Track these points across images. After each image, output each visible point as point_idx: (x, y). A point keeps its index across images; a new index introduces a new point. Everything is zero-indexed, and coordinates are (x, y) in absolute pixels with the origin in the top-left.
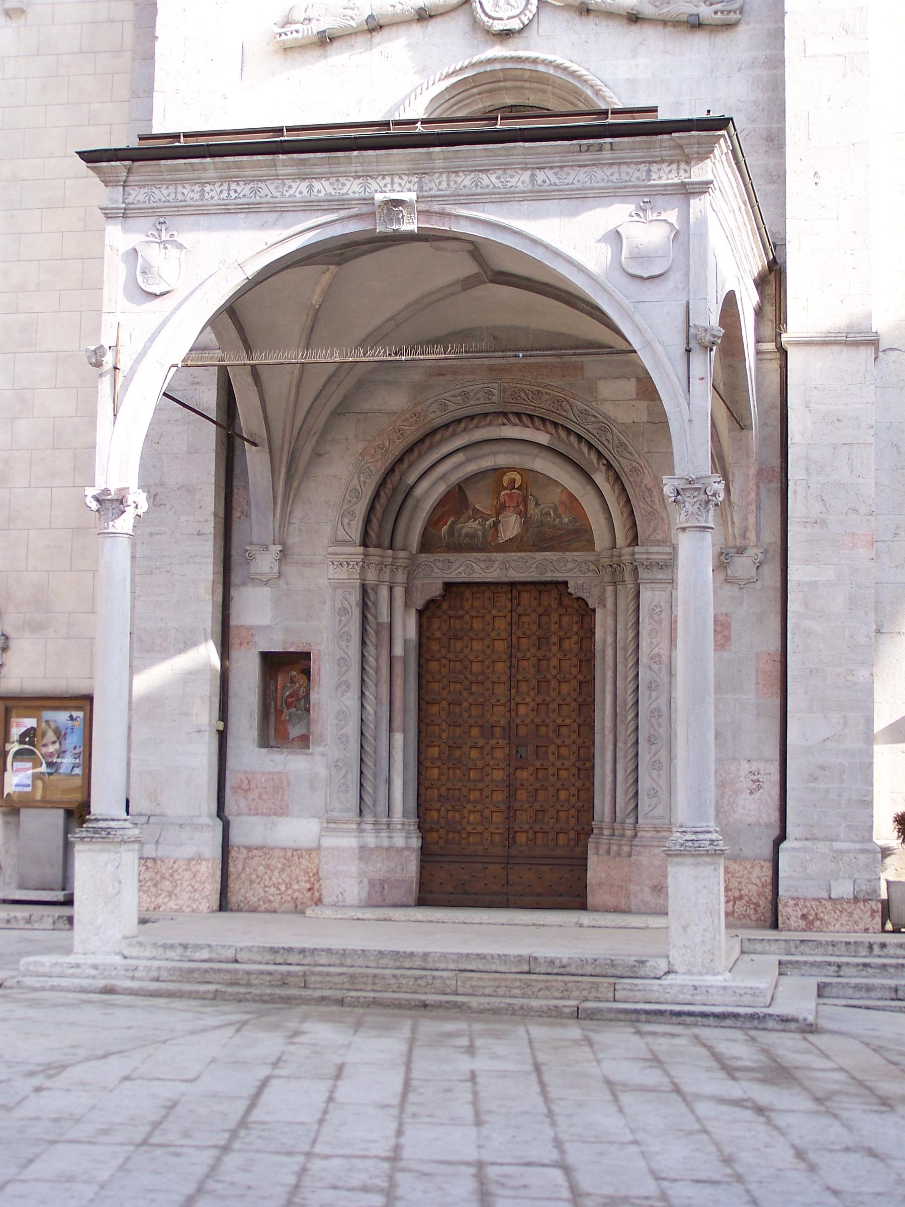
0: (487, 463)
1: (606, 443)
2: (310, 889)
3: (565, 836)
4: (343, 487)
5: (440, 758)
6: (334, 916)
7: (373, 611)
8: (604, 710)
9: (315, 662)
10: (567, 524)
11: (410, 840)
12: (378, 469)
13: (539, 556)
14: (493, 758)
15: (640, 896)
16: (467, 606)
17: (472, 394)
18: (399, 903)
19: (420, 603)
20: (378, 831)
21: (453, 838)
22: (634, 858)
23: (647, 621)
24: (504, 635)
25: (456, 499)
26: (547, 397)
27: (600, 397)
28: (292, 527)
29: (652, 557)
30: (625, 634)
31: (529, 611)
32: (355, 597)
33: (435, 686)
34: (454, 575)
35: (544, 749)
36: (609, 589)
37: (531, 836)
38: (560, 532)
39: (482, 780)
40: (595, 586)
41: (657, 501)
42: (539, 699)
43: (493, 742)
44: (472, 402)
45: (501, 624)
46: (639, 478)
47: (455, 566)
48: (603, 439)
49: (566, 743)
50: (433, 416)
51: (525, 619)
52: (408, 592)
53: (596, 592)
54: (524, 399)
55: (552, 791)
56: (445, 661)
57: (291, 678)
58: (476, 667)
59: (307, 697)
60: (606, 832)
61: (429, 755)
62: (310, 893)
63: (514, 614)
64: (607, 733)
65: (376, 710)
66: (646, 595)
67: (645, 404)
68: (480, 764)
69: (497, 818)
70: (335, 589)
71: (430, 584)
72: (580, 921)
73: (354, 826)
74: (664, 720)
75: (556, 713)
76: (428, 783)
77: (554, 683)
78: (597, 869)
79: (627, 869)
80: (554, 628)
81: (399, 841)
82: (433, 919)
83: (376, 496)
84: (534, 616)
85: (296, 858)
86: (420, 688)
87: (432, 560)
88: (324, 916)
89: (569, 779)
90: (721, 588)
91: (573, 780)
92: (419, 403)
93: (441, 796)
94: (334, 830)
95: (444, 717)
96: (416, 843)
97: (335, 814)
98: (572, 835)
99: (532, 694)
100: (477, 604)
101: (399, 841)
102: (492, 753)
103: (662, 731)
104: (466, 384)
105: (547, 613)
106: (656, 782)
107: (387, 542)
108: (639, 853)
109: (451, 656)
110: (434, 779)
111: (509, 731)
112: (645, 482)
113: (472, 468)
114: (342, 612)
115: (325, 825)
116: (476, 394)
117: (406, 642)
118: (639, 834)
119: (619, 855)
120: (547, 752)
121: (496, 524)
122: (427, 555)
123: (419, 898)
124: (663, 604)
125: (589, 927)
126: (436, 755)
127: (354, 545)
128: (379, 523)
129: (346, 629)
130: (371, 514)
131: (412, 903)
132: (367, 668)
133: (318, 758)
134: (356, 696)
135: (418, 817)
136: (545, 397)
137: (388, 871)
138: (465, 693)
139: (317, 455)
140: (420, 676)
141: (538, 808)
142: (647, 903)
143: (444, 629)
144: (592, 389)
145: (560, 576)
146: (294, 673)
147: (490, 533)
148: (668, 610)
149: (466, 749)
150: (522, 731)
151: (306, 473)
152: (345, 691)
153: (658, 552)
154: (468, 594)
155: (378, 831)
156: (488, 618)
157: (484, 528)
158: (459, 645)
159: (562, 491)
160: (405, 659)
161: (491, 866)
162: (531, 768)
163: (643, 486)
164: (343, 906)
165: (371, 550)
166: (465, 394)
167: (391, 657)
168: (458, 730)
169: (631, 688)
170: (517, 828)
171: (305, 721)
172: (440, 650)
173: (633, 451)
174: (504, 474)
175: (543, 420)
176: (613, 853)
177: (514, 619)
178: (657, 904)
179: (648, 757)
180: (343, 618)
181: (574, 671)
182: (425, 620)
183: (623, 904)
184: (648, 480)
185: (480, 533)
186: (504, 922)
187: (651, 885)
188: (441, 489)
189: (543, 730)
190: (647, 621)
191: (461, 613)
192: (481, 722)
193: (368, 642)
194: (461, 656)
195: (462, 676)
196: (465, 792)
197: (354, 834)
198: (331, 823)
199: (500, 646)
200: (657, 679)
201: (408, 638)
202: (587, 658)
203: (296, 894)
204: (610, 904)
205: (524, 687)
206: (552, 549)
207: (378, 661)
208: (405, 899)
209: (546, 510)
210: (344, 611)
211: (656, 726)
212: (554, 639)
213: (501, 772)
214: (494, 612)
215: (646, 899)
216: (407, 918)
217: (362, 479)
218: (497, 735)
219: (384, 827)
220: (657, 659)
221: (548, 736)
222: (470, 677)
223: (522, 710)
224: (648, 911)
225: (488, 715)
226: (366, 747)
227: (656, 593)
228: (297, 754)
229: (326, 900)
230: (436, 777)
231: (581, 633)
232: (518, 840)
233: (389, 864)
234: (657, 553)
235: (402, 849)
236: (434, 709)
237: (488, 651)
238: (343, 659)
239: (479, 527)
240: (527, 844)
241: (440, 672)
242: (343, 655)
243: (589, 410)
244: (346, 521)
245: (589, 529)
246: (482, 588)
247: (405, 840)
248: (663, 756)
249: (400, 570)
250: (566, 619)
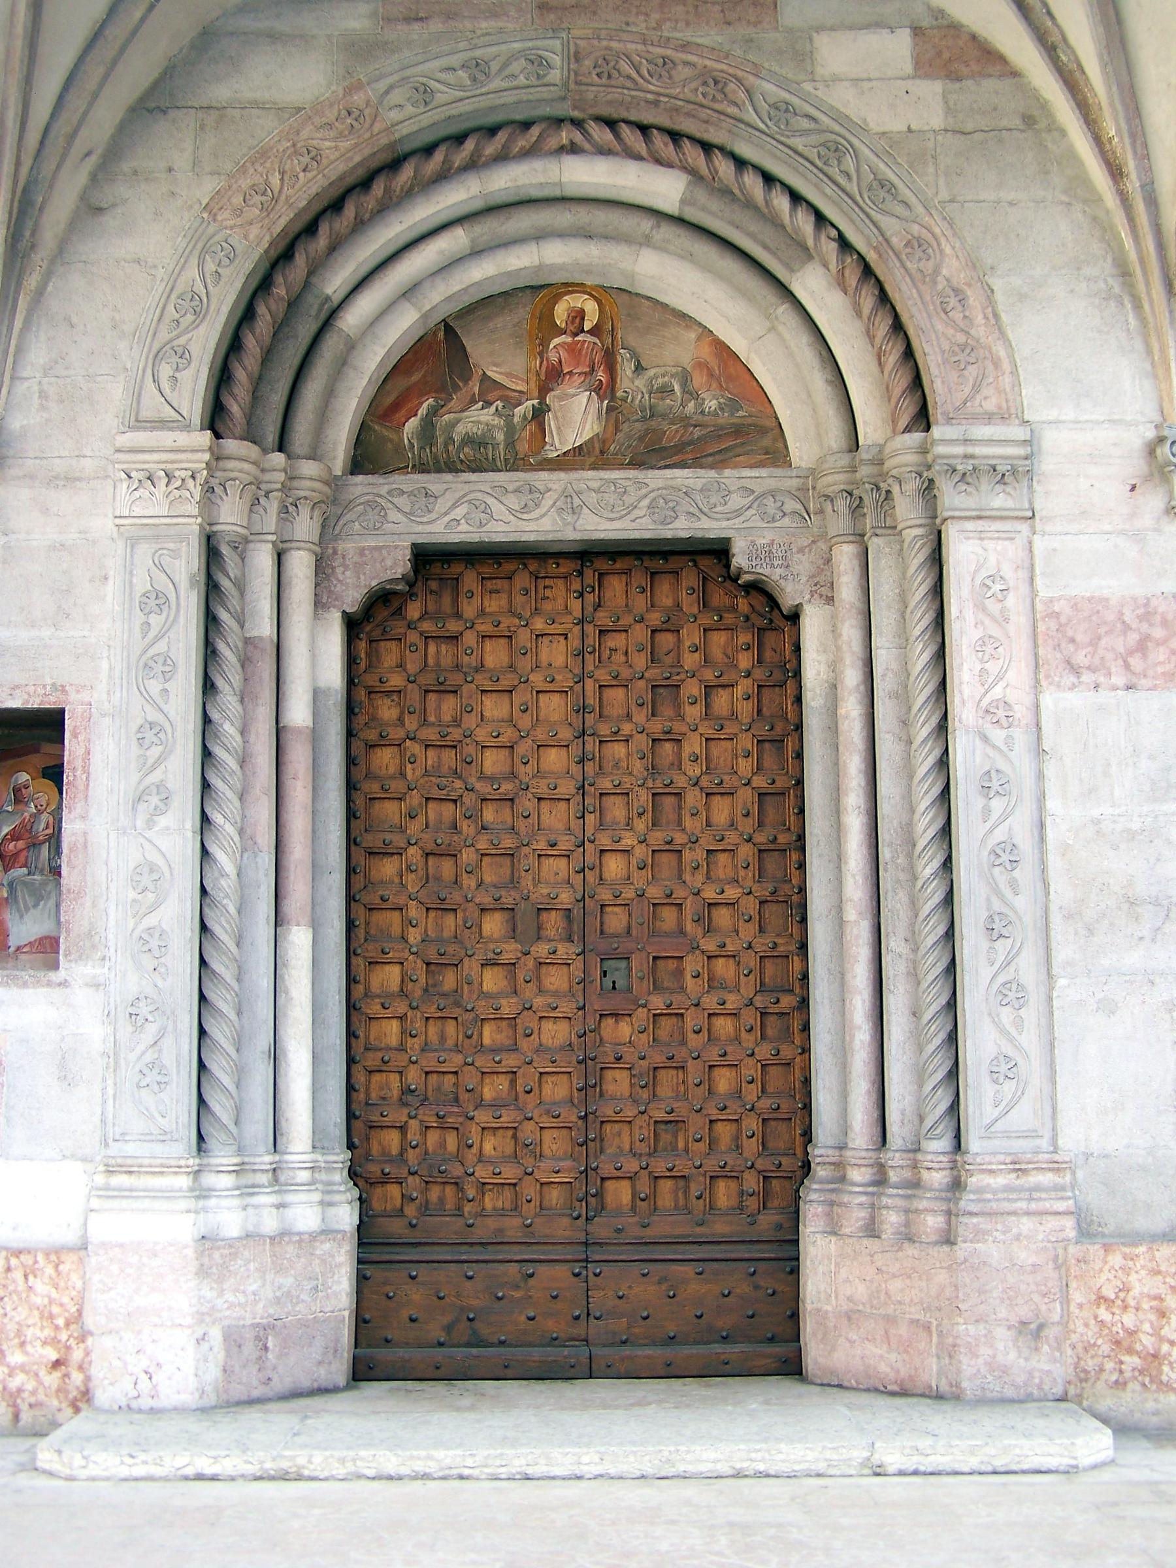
0: (518, 262)
1: (842, 181)
2: (57, 1364)
3: (733, 1184)
4: (160, 287)
5: (403, 993)
6: (124, 1472)
7: (234, 602)
8: (839, 860)
9: (75, 735)
10: (715, 414)
11: (332, 1211)
12: (251, 243)
13: (657, 478)
14: (541, 991)
15: (984, 1351)
16: (469, 610)
17: (494, 66)
18: (306, 1384)
19: (352, 597)
20: (247, 1191)
21: (442, 1200)
22: (963, 1249)
23: (969, 614)
24: (564, 680)
25: (439, 357)
26: (686, 72)
27: (820, 71)
28: (21, 388)
29: (978, 450)
30: (899, 654)
31: (626, 620)
32: (187, 562)
33: (390, 811)
34: (439, 527)
35: (672, 965)
36: (845, 555)
37: (644, 1187)
38: (697, 432)
39: (514, 1049)
40: (801, 550)
41: (979, 319)
42: (657, 838)
43: (541, 950)
44: (496, 84)
45: (556, 654)
46: (931, 264)
47: (441, 505)
48: (834, 171)
49: (730, 947)
50: (395, 115)
51: (616, 641)
52: (322, 568)
53: (803, 565)
54: (629, 77)
55: (694, 1071)
56: (414, 748)
57: (17, 791)
58: (493, 762)
59: (55, 838)
60: (858, 1175)
61: (375, 987)
62: (57, 1374)
63: (589, 629)
64: (851, 914)
65: (241, 866)
66: (962, 551)
67: (937, 86)
68: (508, 1007)
69: (555, 1144)
70: (132, 543)
71: (379, 551)
72: (876, 1459)
73: (184, 1182)
74: (1025, 874)
75: (700, 877)
76: (372, 1060)
77: (693, 798)
78: (834, 1271)
79: (942, 1277)
80: (690, 660)
81: (305, 1214)
82: (432, 1467)
83: (247, 315)
84: (640, 634)
85: (18, 1275)
86: (351, 815)
87: (384, 490)
88: (93, 1471)
89: (737, 1039)
90: (1157, 530)
91: (748, 1040)
92: (358, 87)
93: (407, 1091)
94: (128, 1193)
95: (412, 888)
96: (346, 1216)
97: (130, 1149)
98: (751, 1182)
99: (640, 825)
100: (494, 605)
101: (305, 1214)
102: (538, 978)
103: (1022, 903)
104: (480, 42)
105: (670, 627)
106: (1011, 1040)
107: (271, 437)
108: (979, 1235)
109: (431, 734)
110: (389, 1049)
111: (580, 922)
112: (945, 272)
113: (483, 273)
114: (152, 603)
115: (100, 1180)
116: (505, 66)
117: (317, 694)
118: (973, 1181)
119: (910, 1239)
120: (680, 972)
121: (539, 414)
122: (370, 478)
123: (355, 1360)
124: (1007, 571)
125: (901, 1473)
126: (395, 986)
127: (187, 428)
128: (257, 370)
129: (161, 647)
130: (232, 358)
131: (341, 1379)
132: (217, 750)
133: (80, 995)
134: (188, 825)
135: (351, 1146)
136: (683, 73)
137: (278, 1301)
138: (467, 828)
139: (91, 209)
140: (351, 786)
141: (660, 1115)
142: (1005, 1370)
143: (412, 667)
144: (800, 53)
145: (710, 528)
146: (24, 777)
147: (526, 434)
148: (1024, 589)
149: (471, 967)
150: (616, 920)
151: (61, 251)
152: (158, 812)
153: (992, 440)
154: (470, 580)
155: (247, 1191)
156: (524, 638)
157: (510, 429)
158: (449, 705)
159: (698, 339)
160: (315, 736)
161: (542, 1269)
162: (641, 1013)
163: (941, 284)
164: (152, 1411)
165: (231, 445)
166: (478, 69)
167: (279, 732)
168: (449, 920)
169: (926, 794)
170: (607, 1169)
171: (52, 903)
172: (401, 720)
173: (912, 200)
174: (557, 298)
175: (675, 136)
176: (888, 1231)
177: (589, 641)
178: (1031, 1374)
179: (986, 973)
180: (156, 620)
181: (745, 767)
182: (362, 646)
183: (930, 1372)
184: (952, 268)
185: (500, 436)
186: (649, 1470)
187: (1014, 1321)
188: (403, 326)
189: (668, 916)
190: (969, 614)
191: (453, 626)
192: (508, 900)
193: (220, 683)
194: (456, 734)
195: (458, 784)
196: (470, 1079)
197: (183, 1204)
198: (117, 1171)
199: (554, 707)
200: (1001, 764)
201: (322, 684)
202: (783, 736)
203: (19, 1380)
204: (883, 1368)
205: (616, 810)
206: (697, 463)
207: (245, 734)
208: (322, 1371)
209: (660, 381)
210: (156, 600)
211: (1008, 893)
212: (692, 688)
213: (563, 1026)
214: (539, 624)
215: (1000, 1358)
216: (350, 1467)
217: (210, 266)
218: (551, 933)
219: (264, 1179)
220: (1001, 713)
221: (682, 932)
222: (478, 786)
223: (614, 866)
224: (1009, 1393)
225: (527, 881)
226: (215, 964)
227: (990, 545)
228: (25, 985)
229: (102, 1397)
230: (394, 1041)
231: (759, 674)
232: (609, 1199)
233: (280, 1280)
234: (990, 442)
235: (314, 1237)
236: (388, 868)
237: (525, 722)
238: (152, 725)
239: (497, 421)
240: (633, 1208)
241: (403, 775)
242: (153, 715)
243: (796, 101)
244: (165, 371)
245: (770, 423)
246: (508, 567)
247: (322, 1211)
248: (1027, 968)
249: (305, 511)
250: (719, 639)
